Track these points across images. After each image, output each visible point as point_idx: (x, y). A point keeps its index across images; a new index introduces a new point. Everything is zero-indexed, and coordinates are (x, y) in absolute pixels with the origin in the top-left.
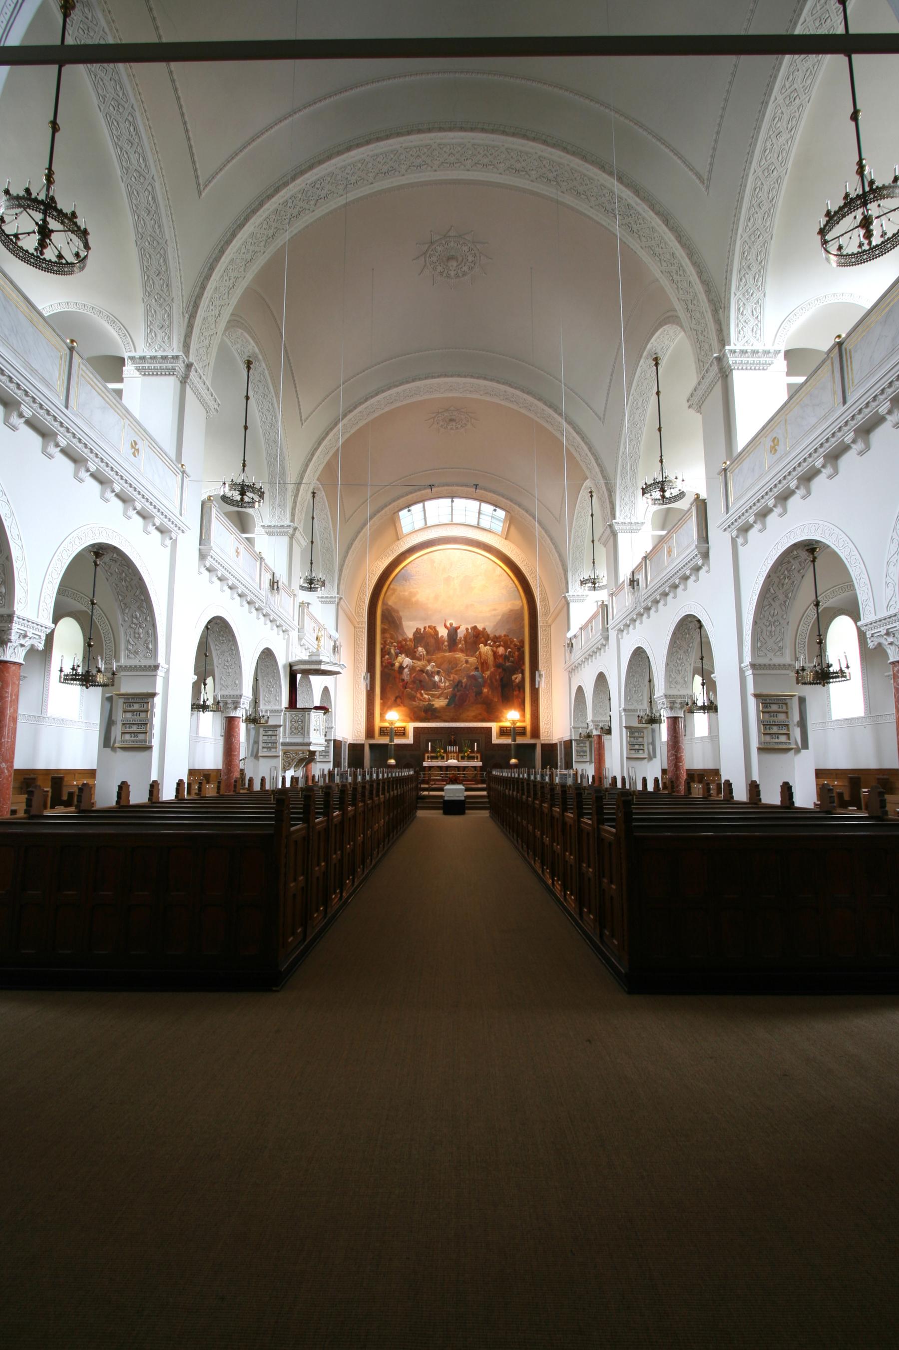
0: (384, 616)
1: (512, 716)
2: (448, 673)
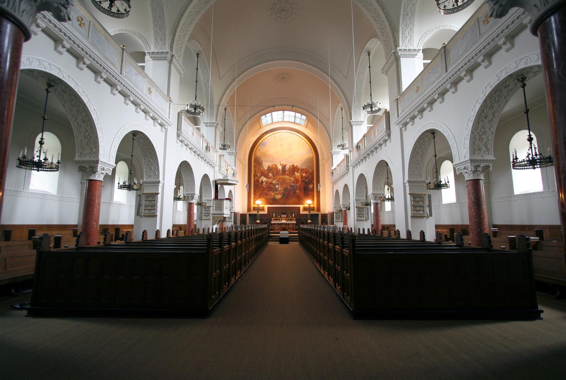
0: (255, 160)
1: (308, 202)
2: (282, 184)
